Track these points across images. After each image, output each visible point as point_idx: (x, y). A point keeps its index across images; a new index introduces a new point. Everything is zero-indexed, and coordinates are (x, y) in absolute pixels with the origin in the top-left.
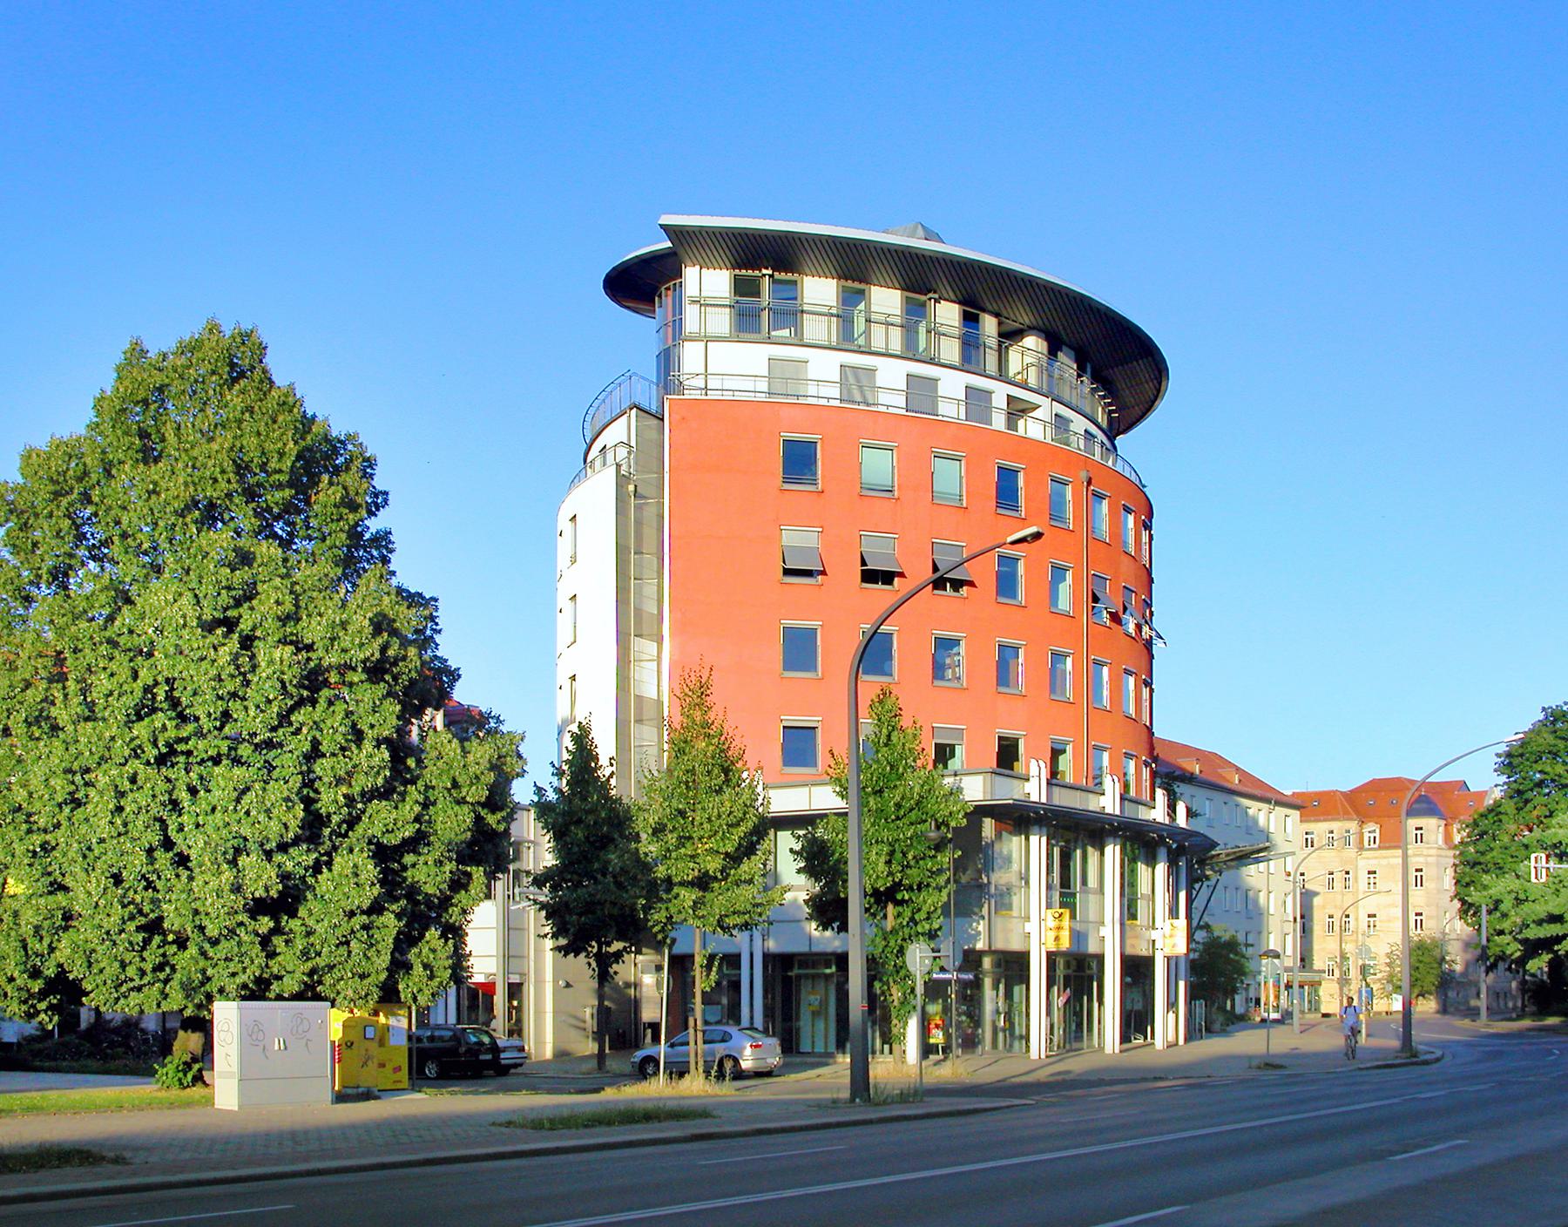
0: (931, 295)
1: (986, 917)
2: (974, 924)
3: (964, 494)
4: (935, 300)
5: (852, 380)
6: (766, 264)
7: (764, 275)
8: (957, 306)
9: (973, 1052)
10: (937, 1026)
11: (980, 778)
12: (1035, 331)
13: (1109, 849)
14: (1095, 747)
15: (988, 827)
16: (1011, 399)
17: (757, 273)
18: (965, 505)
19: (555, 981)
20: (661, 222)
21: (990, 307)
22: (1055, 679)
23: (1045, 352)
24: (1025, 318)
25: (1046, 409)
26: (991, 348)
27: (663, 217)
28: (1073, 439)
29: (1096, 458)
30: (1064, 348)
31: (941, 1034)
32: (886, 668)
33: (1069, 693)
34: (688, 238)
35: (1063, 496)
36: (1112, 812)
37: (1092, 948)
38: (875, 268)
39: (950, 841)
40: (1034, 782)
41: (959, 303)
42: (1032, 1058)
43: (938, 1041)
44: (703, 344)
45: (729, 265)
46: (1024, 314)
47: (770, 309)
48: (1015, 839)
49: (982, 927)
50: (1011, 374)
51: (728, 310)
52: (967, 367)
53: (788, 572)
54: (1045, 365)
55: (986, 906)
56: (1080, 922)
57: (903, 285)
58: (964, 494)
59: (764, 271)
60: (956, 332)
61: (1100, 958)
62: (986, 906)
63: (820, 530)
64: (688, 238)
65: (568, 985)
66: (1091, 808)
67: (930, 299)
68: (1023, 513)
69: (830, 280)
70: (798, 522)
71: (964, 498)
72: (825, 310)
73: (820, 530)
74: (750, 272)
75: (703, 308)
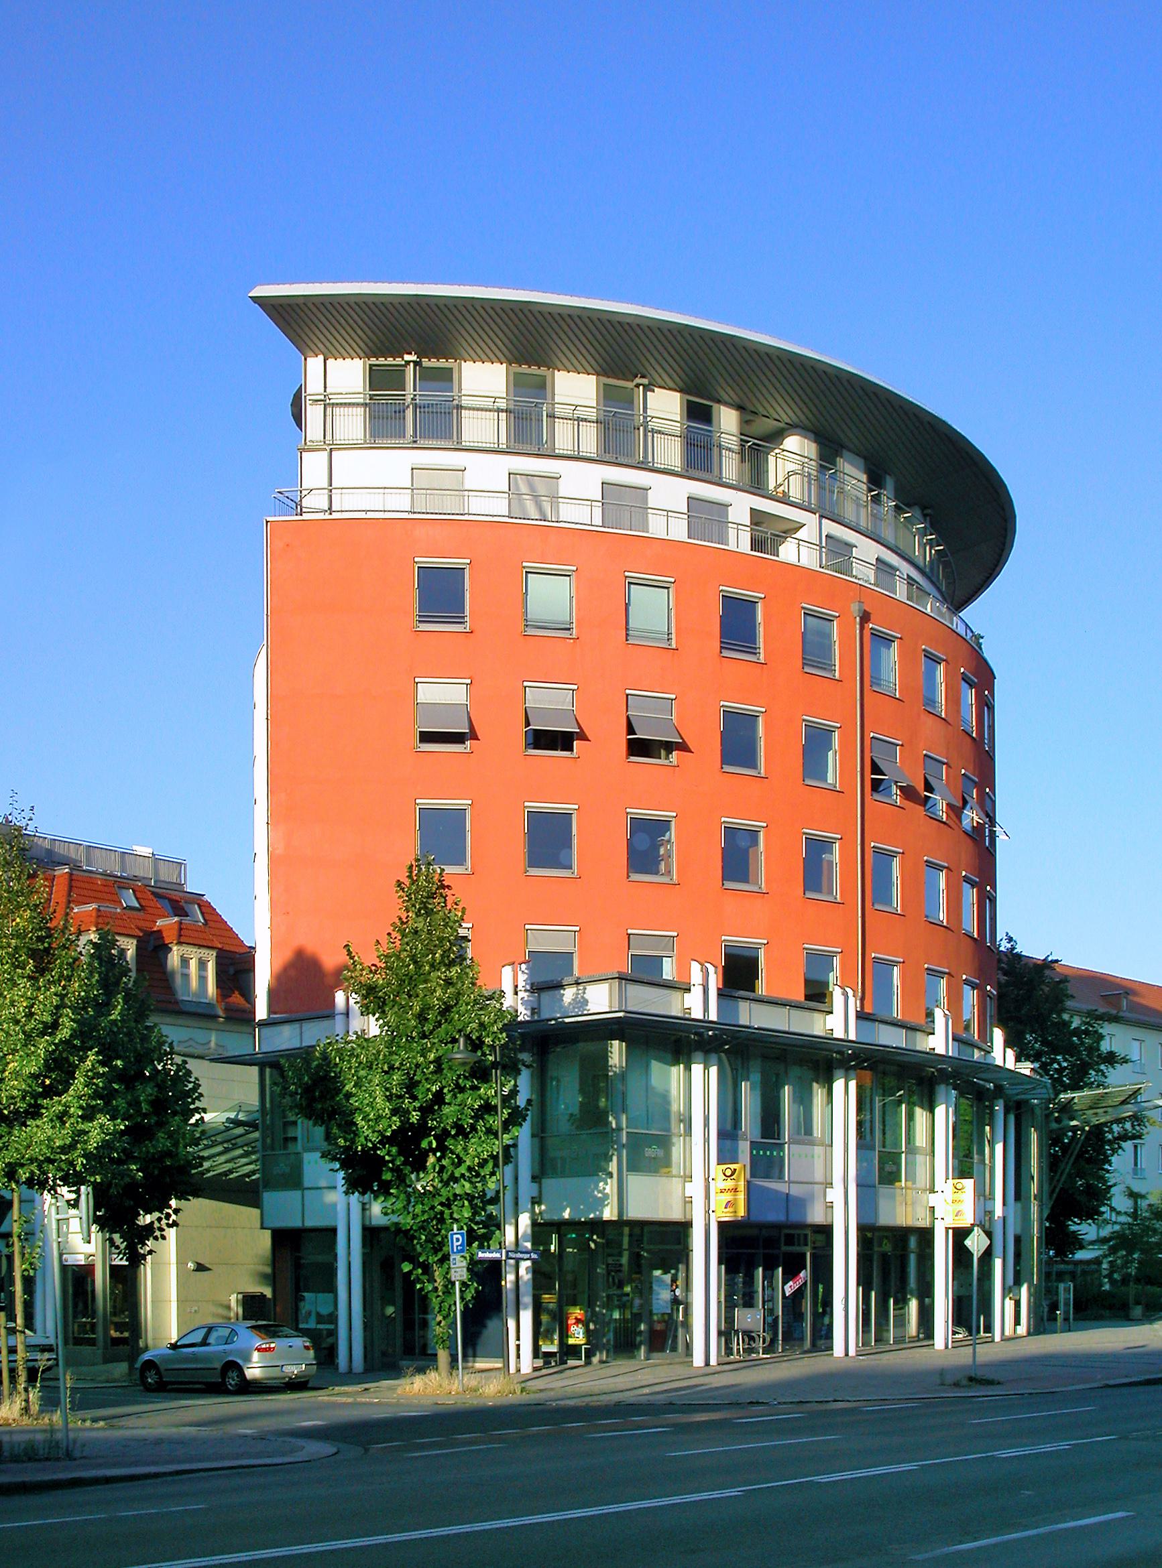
0: (638, 380)
1: (615, 1176)
2: (601, 1184)
3: (673, 631)
4: (644, 386)
5: (524, 489)
6: (409, 349)
7: (408, 363)
8: (678, 394)
9: (634, 1357)
10: (578, 1321)
11: (605, 987)
12: (798, 430)
13: (838, 1085)
14: (876, 960)
15: (617, 1052)
16: (757, 517)
17: (399, 361)
18: (674, 646)
19: (181, 1263)
20: (250, 295)
21: (726, 398)
22: (876, 886)
23: (813, 455)
24: (783, 412)
25: (811, 527)
26: (729, 450)
27: (258, 288)
28: (857, 569)
29: (897, 597)
30: (845, 453)
31: (581, 1331)
32: (562, 856)
33: (897, 903)
34: (299, 311)
35: (829, 636)
36: (700, 1017)
37: (816, 1216)
38: (554, 347)
39: (495, 1065)
40: (696, 994)
41: (681, 391)
42: (695, 1365)
43: (578, 1342)
44: (325, 454)
45: (362, 354)
46: (779, 409)
47: (415, 406)
48: (674, 1069)
49: (609, 1187)
50: (772, 486)
51: (360, 410)
52: (692, 472)
53: (426, 737)
54: (814, 473)
55: (615, 1158)
56: (790, 1182)
57: (599, 369)
58: (673, 631)
59: (407, 357)
60: (677, 428)
61: (826, 1231)
62: (615, 1158)
63: (469, 681)
64: (299, 311)
65: (200, 1268)
66: (816, 1033)
67: (638, 386)
68: (762, 656)
69: (497, 365)
70: (443, 671)
71: (673, 636)
72: (488, 403)
73: (469, 681)
74: (390, 361)
75: (329, 410)
